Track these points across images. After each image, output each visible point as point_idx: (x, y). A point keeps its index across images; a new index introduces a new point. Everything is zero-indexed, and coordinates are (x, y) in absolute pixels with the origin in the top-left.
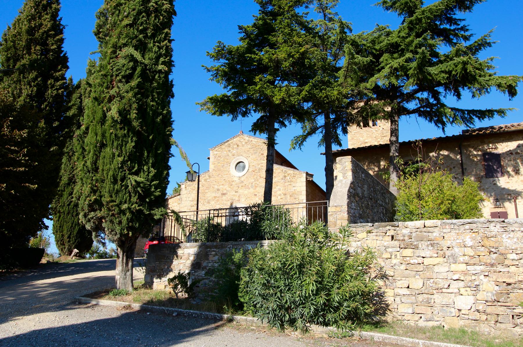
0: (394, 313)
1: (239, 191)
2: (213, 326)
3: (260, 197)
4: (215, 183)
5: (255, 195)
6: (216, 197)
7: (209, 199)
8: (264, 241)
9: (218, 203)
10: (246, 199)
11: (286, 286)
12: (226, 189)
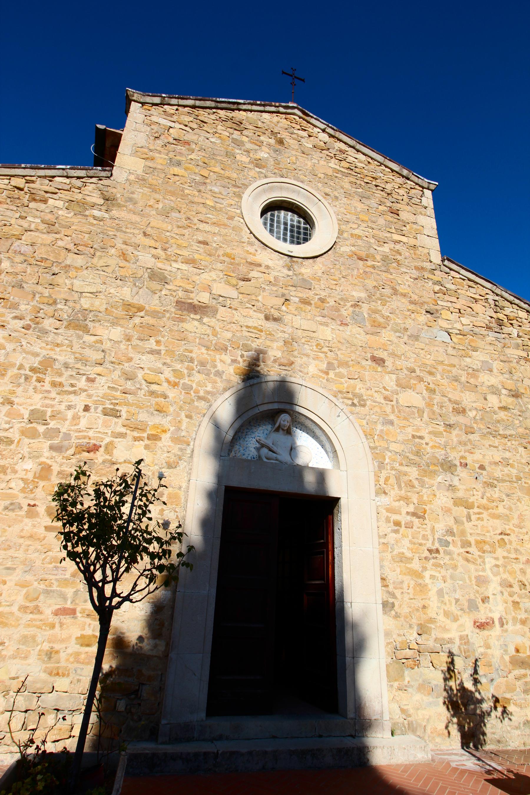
0: (9, 326)
1: (287, 318)
2: (511, 298)
3: (402, 375)
4: (140, 239)
5: (379, 361)
6: (140, 309)
7: (85, 303)
8: (413, 511)
9: (152, 344)
10: (330, 366)
11: (276, 278)
12: (208, 288)
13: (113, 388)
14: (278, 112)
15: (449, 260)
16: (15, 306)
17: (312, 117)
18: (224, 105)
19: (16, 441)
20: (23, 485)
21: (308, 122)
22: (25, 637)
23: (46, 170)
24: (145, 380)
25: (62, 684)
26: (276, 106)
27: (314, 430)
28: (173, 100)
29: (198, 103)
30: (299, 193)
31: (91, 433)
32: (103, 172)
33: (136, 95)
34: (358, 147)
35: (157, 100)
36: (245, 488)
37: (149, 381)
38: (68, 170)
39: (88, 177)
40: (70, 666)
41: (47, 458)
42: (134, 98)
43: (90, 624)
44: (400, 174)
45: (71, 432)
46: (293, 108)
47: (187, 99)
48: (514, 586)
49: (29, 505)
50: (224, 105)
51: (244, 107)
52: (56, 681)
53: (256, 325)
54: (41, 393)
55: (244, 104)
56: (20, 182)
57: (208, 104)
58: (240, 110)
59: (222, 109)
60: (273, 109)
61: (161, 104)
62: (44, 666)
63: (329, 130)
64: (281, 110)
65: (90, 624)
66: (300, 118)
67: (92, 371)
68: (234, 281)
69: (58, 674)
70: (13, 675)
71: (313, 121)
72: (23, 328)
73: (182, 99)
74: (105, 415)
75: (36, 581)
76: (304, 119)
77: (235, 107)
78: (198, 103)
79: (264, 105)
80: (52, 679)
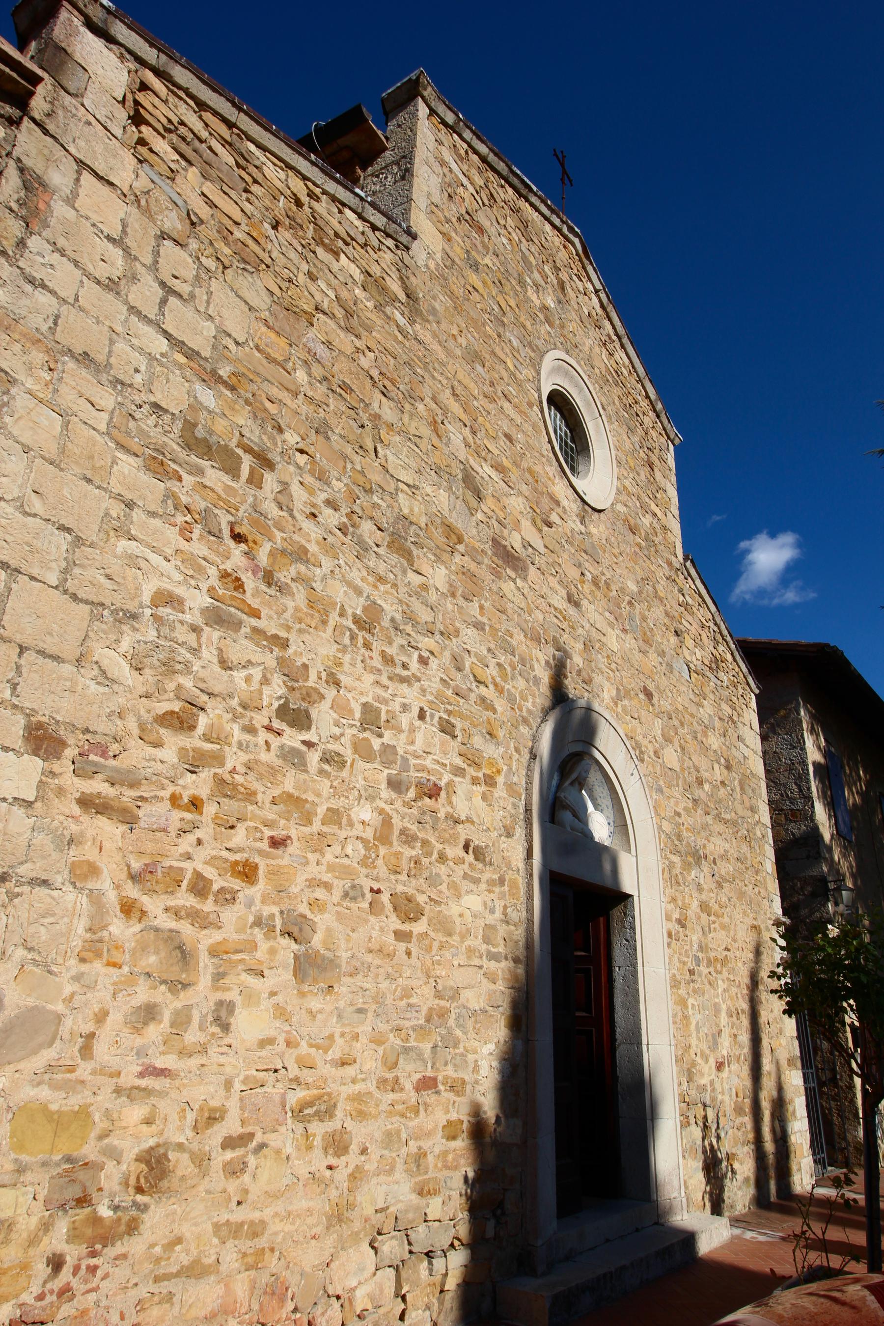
13: (445, 681)
14: (559, 230)
15: (692, 562)
16: (322, 477)
17: (591, 264)
18: (516, 181)
19: (349, 763)
20: (363, 852)
21: (584, 268)
22: (388, 1134)
23: (339, 187)
24: (475, 676)
25: (435, 1207)
26: (562, 221)
27: (596, 787)
28: (468, 131)
29: (491, 158)
30: (581, 391)
31: (428, 762)
32: (405, 235)
33: (429, 89)
34: (625, 340)
35: (450, 118)
36: (564, 875)
37: (479, 678)
38: (367, 205)
39: (385, 232)
40: (439, 1175)
41: (386, 802)
42: (425, 93)
43: (454, 1102)
44: (653, 407)
45: (409, 757)
46: (576, 235)
47: (483, 142)
48: (334, 891)
49: (372, 890)
50: (516, 181)
51: (534, 199)
52: (428, 1205)
53: (560, 607)
54: (371, 672)
55: (536, 195)
56: (298, 186)
57: (501, 166)
58: (527, 200)
59: (511, 185)
60: (557, 222)
61: (451, 128)
62: (413, 1180)
63: (603, 295)
64: (565, 229)
65: (454, 1102)
66: (578, 254)
67: (426, 642)
68: (539, 522)
69: (429, 1193)
70: (380, 1205)
71: (590, 269)
72: (340, 529)
73: (479, 138)
74: (442, 731)
75: (391, 1031)
76: (581, 260)
77: (524, 192)
78: (491, 158)
79: (553, 211)
80: (423, 1202)
